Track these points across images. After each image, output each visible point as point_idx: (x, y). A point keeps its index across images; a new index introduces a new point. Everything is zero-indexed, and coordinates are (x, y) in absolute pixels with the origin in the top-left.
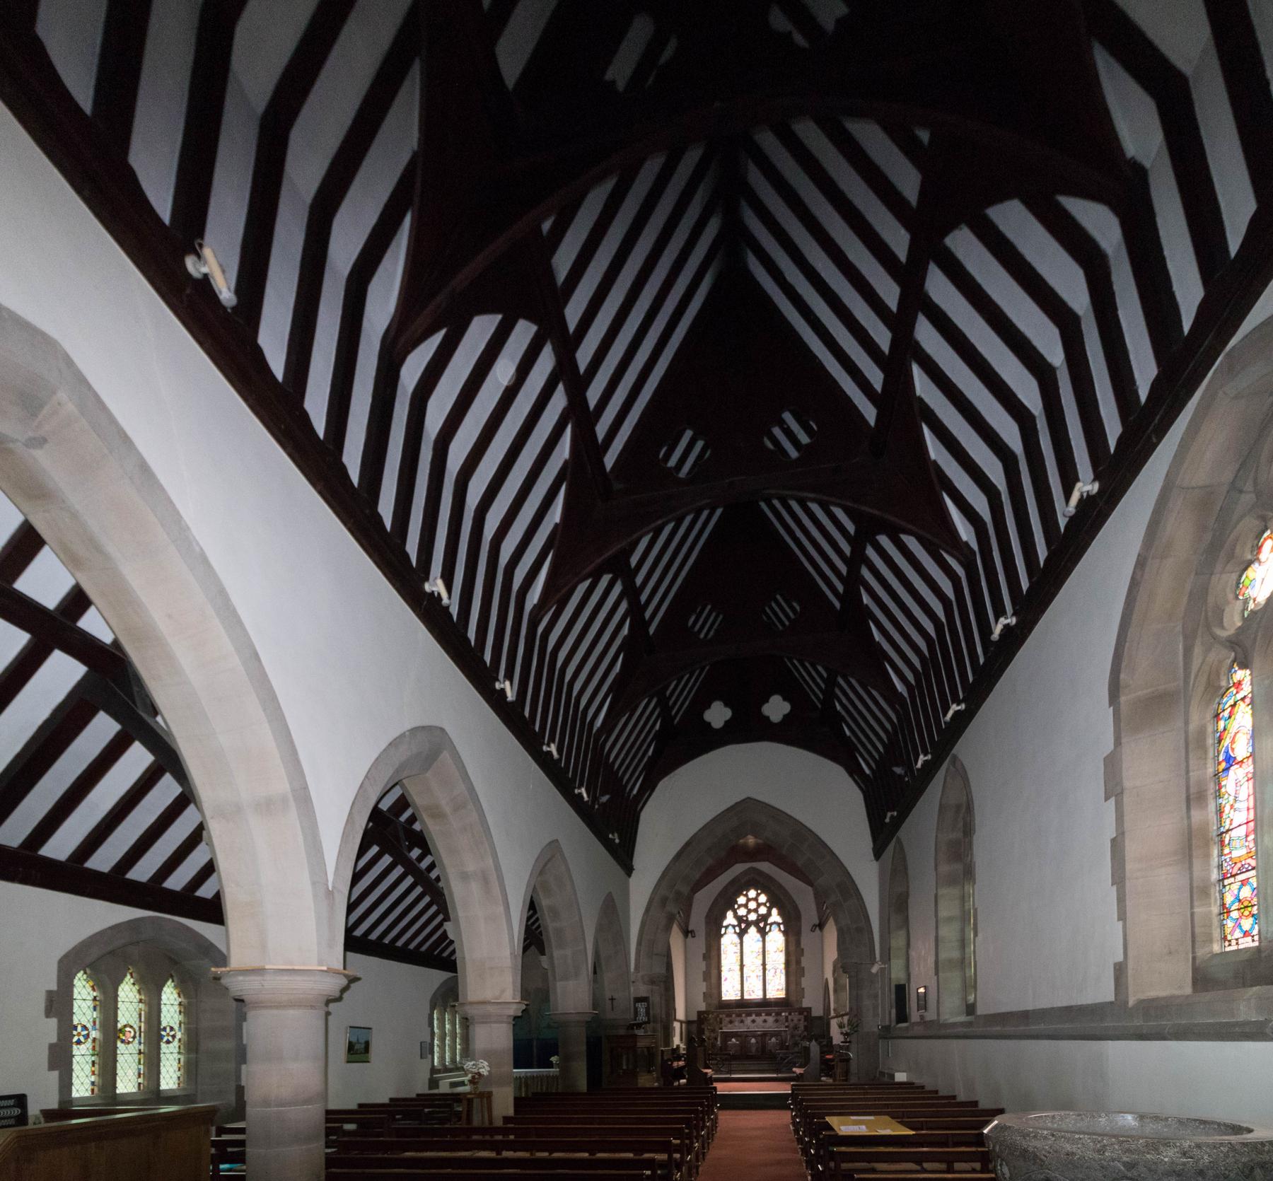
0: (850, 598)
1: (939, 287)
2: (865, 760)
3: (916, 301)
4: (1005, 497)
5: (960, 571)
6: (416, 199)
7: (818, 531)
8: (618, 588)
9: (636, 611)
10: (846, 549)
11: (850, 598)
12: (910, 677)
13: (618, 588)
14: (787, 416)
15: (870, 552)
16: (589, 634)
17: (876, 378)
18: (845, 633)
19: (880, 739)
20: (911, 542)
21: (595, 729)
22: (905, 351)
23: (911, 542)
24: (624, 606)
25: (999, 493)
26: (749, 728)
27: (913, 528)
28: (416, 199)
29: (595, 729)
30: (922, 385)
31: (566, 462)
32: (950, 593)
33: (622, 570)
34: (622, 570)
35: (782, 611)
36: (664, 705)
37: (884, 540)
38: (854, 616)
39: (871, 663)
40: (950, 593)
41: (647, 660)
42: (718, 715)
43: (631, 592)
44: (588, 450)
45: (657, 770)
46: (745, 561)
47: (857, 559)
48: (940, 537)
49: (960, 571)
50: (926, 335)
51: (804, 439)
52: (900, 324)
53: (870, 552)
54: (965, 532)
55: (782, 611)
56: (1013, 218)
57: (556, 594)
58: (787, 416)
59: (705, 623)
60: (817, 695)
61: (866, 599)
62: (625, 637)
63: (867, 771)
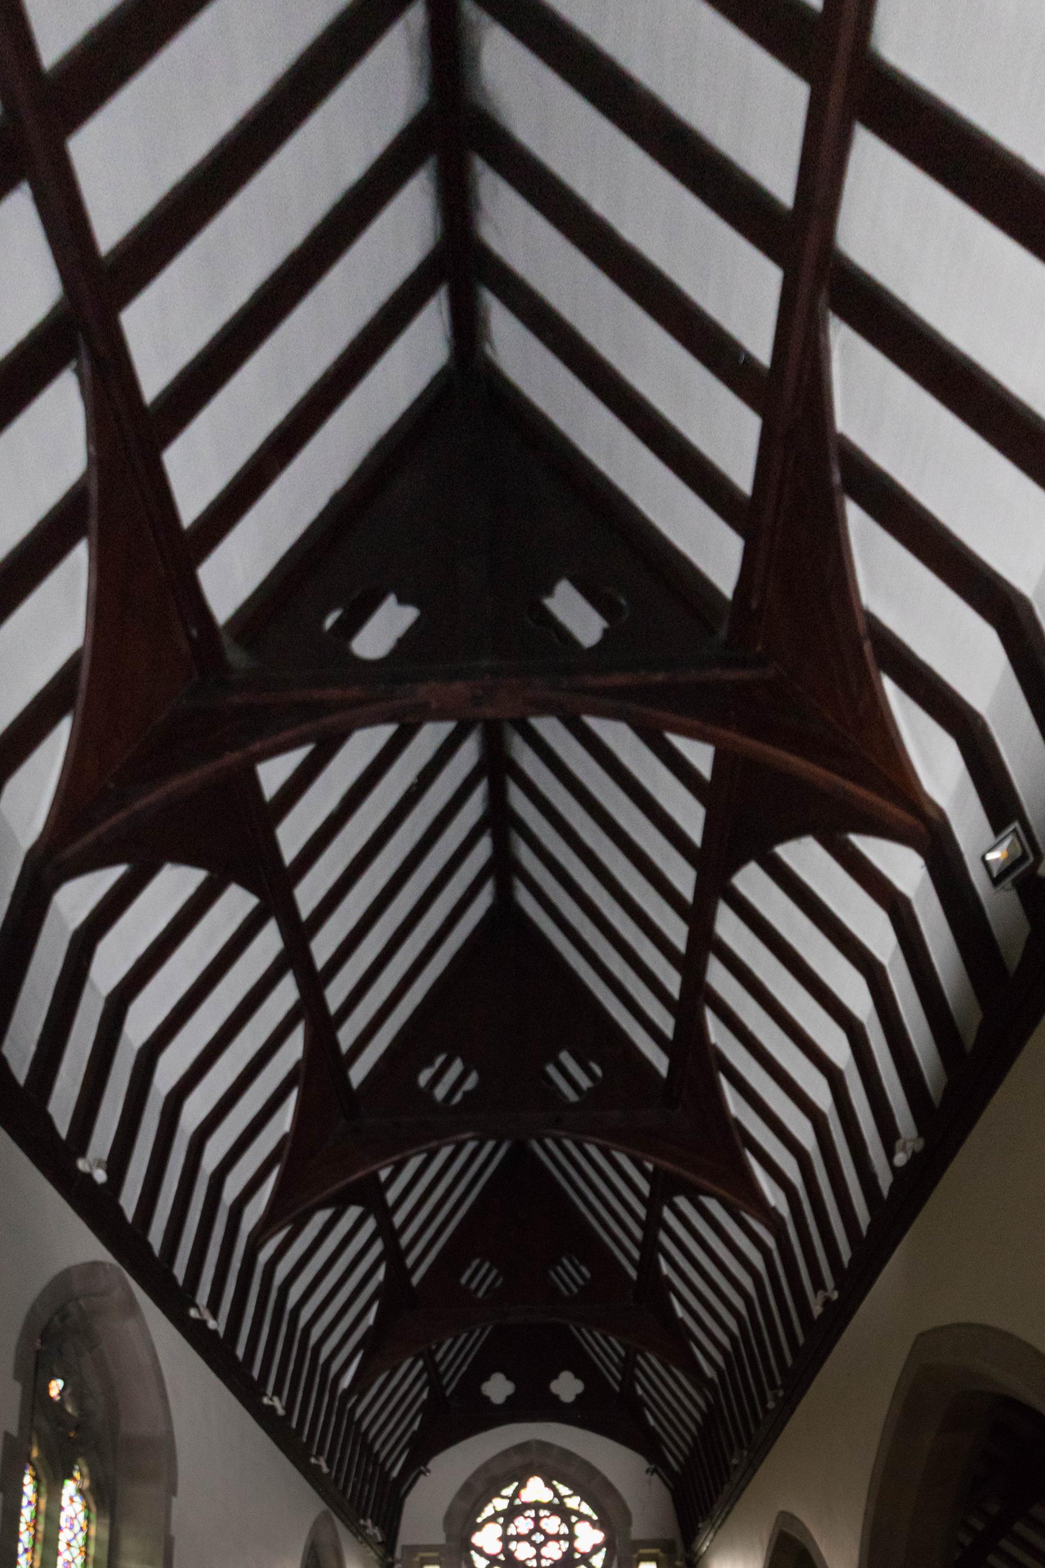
0: (647, 1266)
1: (728, 927)
2: (670, 1452)
3: (704, 942)
4: (776, 1255)
5: (770, 1241)
6: (93, 523)
7: (607, 1184)
8: (370, 1225)
9: (394, 1255)
10: (642, 1212)
11: (647, 1266)
12: (689, 1439)
13: (370, 1225)
14: (565, 1057)
15: (667, 1214)
16: (329, 1271)
17: (666, 1023)
18: (642, 1305)
19: (696, 1404)
20: (713, 1206)
21: (340, 1391)
22: (696, 997)
23: (713, 1206)
24: (378, 1247)
25: (745, 1322)
26: (533, 1403)
27: (716, 1189)
28: (93, 523)
29: (340, 1391)
30: (716, 1032)
31: (285, 1137)
32: (743, 1311)
33: (370, 1196)
34: (370, 1196)
35: (571, 1275)
36: (431, 1367)
37: (683, 1203)
38: (654, 1289)
39: (676, 1344)
40: (743, 1311)
41: (404, 1315)
42: (498, 1388)
43: (387, 1232)
44: (324, 1062)
45: (422, 1450)
46: (522, 1215)
47: (653, 1224)
48: (745, 1198)
49: (770, 1241)
50: (718, 977)
51: (585, 1083)
52: (690, 965)
53: (667, 1214)
54: (774, 1196)
55: (571, 1275)
56: (806, 856)
57: (287, 1212)
58: (565, 1057)
59: (479, 1277)
60: (614, 1378)
61: (665, 1268)
62: (370, 1329)
63: (676, 1467)
